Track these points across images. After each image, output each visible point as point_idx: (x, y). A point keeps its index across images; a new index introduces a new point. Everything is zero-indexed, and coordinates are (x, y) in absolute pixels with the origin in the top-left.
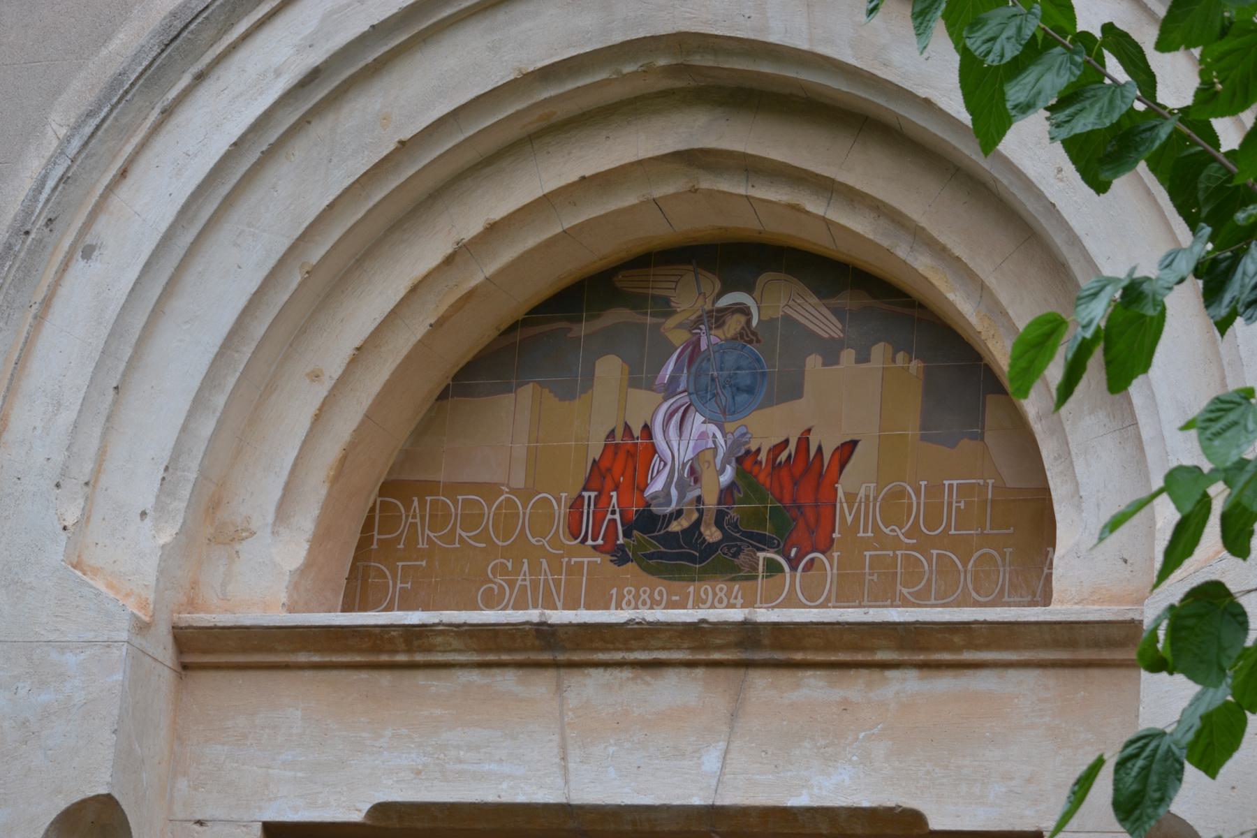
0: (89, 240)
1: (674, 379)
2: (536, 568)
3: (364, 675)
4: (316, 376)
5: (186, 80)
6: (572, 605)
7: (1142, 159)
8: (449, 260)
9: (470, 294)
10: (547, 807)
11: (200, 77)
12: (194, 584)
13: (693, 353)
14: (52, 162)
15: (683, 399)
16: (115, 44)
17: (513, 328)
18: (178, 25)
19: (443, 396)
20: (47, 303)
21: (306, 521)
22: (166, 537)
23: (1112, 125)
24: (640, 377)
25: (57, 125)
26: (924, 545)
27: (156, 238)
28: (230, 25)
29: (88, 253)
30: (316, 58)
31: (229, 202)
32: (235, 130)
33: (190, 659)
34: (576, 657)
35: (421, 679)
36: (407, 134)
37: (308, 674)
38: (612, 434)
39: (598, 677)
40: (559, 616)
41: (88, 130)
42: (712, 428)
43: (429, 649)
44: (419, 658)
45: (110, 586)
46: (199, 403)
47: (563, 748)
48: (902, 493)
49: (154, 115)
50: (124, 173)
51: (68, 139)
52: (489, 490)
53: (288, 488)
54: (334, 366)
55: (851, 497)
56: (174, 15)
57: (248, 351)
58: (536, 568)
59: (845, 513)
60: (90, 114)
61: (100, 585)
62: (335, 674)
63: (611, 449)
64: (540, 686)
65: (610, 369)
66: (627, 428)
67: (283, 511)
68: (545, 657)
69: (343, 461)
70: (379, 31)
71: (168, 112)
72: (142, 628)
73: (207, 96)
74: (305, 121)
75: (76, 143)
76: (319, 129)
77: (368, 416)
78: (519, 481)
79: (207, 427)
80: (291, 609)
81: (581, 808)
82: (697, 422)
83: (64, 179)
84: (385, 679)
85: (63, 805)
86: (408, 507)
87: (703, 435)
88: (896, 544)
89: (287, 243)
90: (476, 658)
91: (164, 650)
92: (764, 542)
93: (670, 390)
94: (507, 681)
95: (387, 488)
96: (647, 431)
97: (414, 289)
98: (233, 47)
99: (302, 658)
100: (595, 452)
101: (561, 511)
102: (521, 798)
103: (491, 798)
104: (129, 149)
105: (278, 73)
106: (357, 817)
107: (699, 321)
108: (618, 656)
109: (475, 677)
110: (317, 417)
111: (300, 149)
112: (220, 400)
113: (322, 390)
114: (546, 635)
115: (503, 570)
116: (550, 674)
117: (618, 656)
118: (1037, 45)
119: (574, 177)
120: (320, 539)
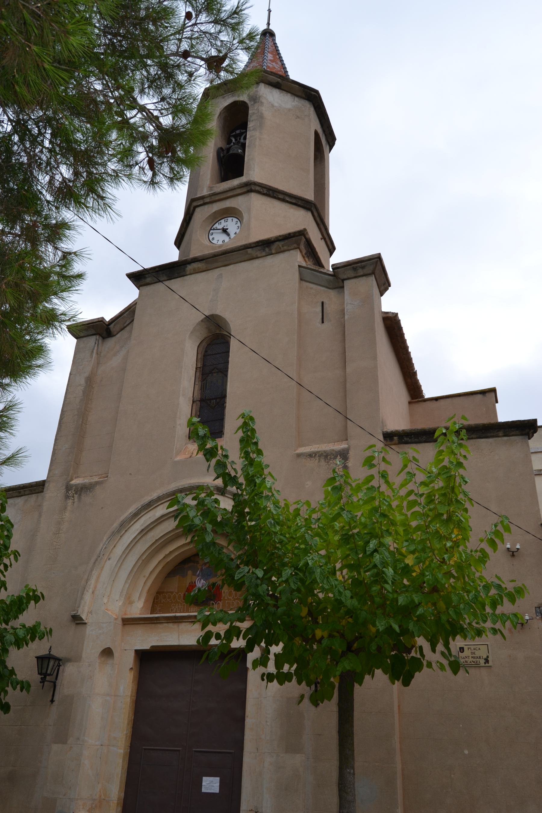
0: (109, 557)
1: (199, 574)
2: (178, 605)
3: (150, 625)
4: (144, 576)
5: (124, 532)
6: (180, 612)
7: (365, 674)
8: (164, 557)
9: (168, 562)
10: (176, 645)
11: (126, 531)
12: (126, 611)
13: (202, 569)
14: (104, 545)
15: (200, 577)
16: (114, 526)
17: (176, 566)
18: (122, 523)
19: (166, 577)
20: (103, 567)
21: (143, 600)
22: (120, 604)
23: (199, 103)
24: (194, 574)
25: (105, 539)
26: (234, 600)
27: (119, 557)
28: (130, 523)
29: (109, 559)
30: (143, 528)
31: (130, 550)
32: (131, 539)
33: (125, 623)
34: (181, 621)
35: (158, 625)
36: (157, 539)
37: (142, 625)
38: (190, 583)
39: (184, 624)
40: (178, 614)
41: (109, 540)
42: (204, 582)
43: (159, 620)
44: (158, 622)
45: (111, 612)
46: (126, 582)
47: (179, 635)
48: (232, 592)
49: (119, 537)
50: (115, 546)
51: (106, 542)
52: (172, 593)
53: (140, 595)
54: (147, 575)
55: (224, 592)
56: (122, 521)
57: (134, 573)
58: (178, 605)
59: (223, 595)
60: (109, 538)
61: (110, 613)
62: (146, 625)
63: (190, 586)
64: (175, 626)
65: (190, 572)
66: (192, 582)
67: (139, 598)
68: (176, 621)
69: (149, 589)
70: (152, 523)
71: (121, 537)
72: (116, 619)
73: (127, 533)
74: (142, 537)
75: (107, 542)
76: (144, 538)
77: (153, 582)
78: (176, 591)
79: (127, 586)
80: (140, 614)
81: (181, 645)
82: (202, 581)
83: (105, 548)
84: (153, 625)
85: (102, 649)
86: (160, 595)
87: (203, 583)
88: (230, 600)
89: (139, 556)
90: (166, 621)
91: (120, 622)
92: (211, 600)
93: (198, 576)
94: (171, 625)
95: (157, 593)
96: (195, 582)
97: (159, 562)
98: (131, 526)
99: (141, 622)
100: (187, 586)
101: (182, 595)
102: (172, 644)
103: (168, 644)
104: (115, 543)
105: (137, 530)
106: (148, 648)
107: (202, 565)
108: (187, 620)
109: (166, 624)
110: (145, 583)
111: (141, 541)
112: (129, 581)
113: (145, 579)
114: (176, 618)
115: (174, 606)
116: (177, 624)
117: (187, 620)
118: (403, 679)
119: (182, 544)
120: (146, 601)
